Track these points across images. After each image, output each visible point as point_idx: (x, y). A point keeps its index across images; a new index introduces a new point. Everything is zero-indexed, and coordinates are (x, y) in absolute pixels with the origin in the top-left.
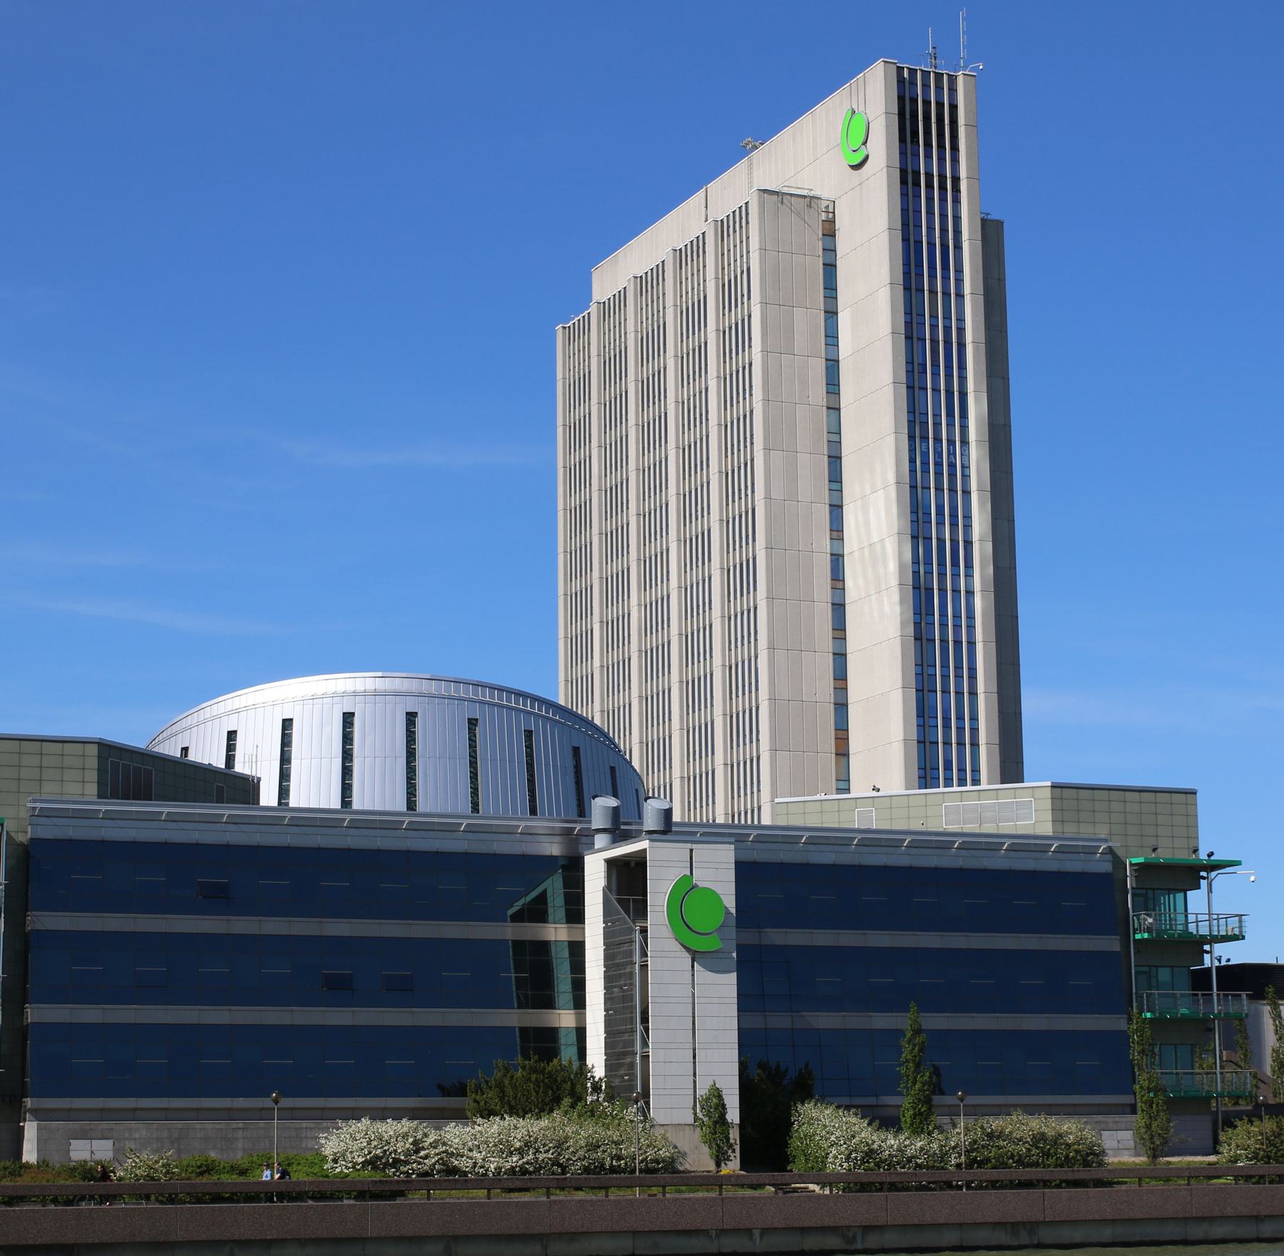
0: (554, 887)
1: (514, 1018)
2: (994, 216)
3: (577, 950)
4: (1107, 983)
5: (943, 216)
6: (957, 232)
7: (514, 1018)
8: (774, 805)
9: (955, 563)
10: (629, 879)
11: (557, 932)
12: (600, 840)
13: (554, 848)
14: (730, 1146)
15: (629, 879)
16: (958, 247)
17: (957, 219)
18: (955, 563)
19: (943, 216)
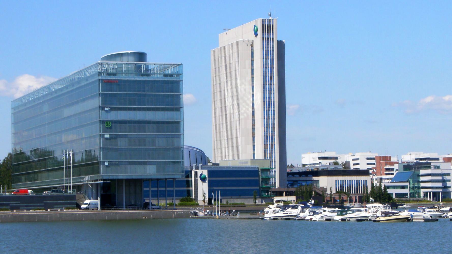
0: (190, 173)
1: (186, 189)
2: (279, 40)
3: (192, 181)
4: (256, 183)
5: (270, 45)
6: (273, 48)
7: (186, 189)
8: (148, 191)
9: (271, 105)
10: (196, 173)
11: (190, 179)
12: (194, 169)
13: (190, 170)
14: (320, 163)
15: (196, 173)
16: (273, 50)
17: (273, 45)
18: (271, 105)
19: (270, 45)
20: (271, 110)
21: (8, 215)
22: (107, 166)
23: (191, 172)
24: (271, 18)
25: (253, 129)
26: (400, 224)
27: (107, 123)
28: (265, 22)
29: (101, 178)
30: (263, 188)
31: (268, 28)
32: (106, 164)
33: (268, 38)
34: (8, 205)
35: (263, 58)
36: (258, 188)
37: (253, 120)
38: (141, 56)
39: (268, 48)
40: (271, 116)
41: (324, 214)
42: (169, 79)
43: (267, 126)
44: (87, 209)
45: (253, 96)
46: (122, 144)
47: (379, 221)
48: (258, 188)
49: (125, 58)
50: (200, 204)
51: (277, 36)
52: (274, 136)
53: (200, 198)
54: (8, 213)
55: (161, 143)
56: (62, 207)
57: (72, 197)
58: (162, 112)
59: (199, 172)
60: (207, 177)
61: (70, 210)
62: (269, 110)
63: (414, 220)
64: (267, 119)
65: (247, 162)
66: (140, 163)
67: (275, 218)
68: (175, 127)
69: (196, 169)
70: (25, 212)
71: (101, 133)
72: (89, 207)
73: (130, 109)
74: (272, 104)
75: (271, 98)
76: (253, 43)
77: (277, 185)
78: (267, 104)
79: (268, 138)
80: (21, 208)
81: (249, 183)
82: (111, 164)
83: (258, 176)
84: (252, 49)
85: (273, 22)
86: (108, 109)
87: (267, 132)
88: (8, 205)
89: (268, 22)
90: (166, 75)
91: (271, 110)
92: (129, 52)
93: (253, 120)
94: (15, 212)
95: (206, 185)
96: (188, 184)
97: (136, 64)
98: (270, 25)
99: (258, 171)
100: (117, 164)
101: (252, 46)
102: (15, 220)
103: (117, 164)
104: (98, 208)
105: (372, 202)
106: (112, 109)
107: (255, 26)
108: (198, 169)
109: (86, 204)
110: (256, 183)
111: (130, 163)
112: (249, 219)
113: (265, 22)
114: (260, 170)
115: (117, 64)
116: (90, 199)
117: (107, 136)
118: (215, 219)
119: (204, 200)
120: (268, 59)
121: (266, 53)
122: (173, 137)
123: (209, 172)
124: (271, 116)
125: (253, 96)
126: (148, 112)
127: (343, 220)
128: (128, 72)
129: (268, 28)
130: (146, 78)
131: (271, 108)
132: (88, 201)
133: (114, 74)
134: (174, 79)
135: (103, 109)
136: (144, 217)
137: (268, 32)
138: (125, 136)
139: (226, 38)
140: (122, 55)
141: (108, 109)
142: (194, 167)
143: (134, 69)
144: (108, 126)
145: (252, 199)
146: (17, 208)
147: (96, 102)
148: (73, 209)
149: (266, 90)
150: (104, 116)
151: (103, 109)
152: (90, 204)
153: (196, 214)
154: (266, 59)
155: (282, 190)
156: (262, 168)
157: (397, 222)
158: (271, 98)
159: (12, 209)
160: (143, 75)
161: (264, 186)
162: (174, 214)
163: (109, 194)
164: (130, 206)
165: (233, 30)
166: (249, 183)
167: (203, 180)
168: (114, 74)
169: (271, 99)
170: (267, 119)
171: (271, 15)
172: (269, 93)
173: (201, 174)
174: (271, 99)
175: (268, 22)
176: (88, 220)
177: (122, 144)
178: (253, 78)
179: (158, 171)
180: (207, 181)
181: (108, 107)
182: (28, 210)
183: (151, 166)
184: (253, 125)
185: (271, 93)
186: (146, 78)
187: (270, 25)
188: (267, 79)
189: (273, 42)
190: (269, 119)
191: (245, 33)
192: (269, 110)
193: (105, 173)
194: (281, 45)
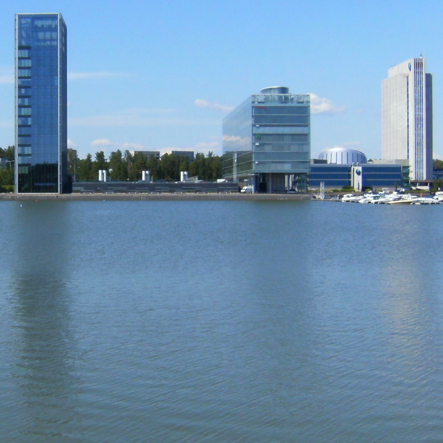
2: (428, 73)
4: (399, 176)
10: (354, 169)
12: (353, 166)
13: (350, 167)
15: (354, 169)
20: (421, 124)
21: (191, 196)
22: (257, 164)
23: (351, 168)
24: (421, 58)
25: (408, 137)
26: (406, 206)
27: (257, 135)
28: (417, 60)
29: (253, 172)
30: (404, 180)
31: (418, 65)
32: (257, 163)
33: (418, 72)
34: (194, 189)
35: (415, 86)
36: (400, 180)
37: (408, 131)
38: (284, 90)
39: (419, 79)
40: (421, 128)
41: (368, 198)
42: (262, 105)
43: (417, 135)
44: (245, 192)
45: (408, 113)
46: (268, 149)
47: (390, 204)
48: (400, 180)
49: (272, 91)
50: (356, 191)
51: (426, 70)
52: (423, 142)
53: (356, 187)
54: (193, 194)
55: (294, 149)
56: (229, 191)
57: (236, 185)
58: (270, 128)
59: (356, 168)
60: (361, 171)
61: (234, 193)
62: (419, 124)
63: (416, 204)
64: (417, 130)
65: (393, 162)
66: (280, 162)
67: (348, 201)
68: (305, 138)
69: (354, 166)
70: (204, 194)
71: (253, 142)
72: (246, 191)
73: (273, 126)
74: (422, 119)
75: (421, 115)
76: (408, 75)
77: (425, 178)
78: (418, 120)
79: (418, 144)
80: (156, 190)
81: (394, 176)
82: (260, 163)
83: (400, 171)
84: (408, 80)
85: (422, 60)
86: (258, 126)
87: (417, 139)
88: (194, 189)
89: (418, 60)
90: (299, 103)
91: (421, 124)
92: (275, 87)
93: (408, 131)
94: (198, 194)
95: (360, 177)
96: (349, 176)
97: (278, 95)
98: (418, 63)
99: (400, 168)
100: (264, 163)
101: (408, 78)
102: (226, 199)
103: (264, 163)
104: (252, 192)
105: (440, 191)
106: (260, 126)
107: (409, 64)
108: (356, 166)
109: (244, 189)
110: (399, 176)
111: (273, 162)
112: (336, 201)
113: (417, 60)
114: (401, 167)
115: (265, 95)
116: (247, 186)
117: (257, 144)
118: (321, 201)
119: (358, 188)
120: (419, 87)
121: (417, 83)
122: (303, 144)
123: (363, 168)
124: (421, 128)
125: (408, 113)
126: (292, 128)
127: (376, 203)
128: (274, 101)
129: (418, 65)
130: (284, 105)
131: (421, 122)
132: (245, 188)
133: (263, 103)
134: (304, 105)
135: (255, 125)
136: (281, 199)
137: (418, 68)
138: (269, 144)
139: (393, 72)
140: (271, 89)
141: (258, 126)
142: (353, 164)
143: (276, 98)
144: (257, 137)
145: (394, 188)
146: (200, 191)
147: (250, 122)
148: (235, 192)
149: (417, 109)
150: (256, 131)
151: (255, 125)
152: (246, 189)
153: (315, 197)
154: (417, 87)
155: (427, 181)
156: (403, 165)
157: (400, 205)
158: (421, 115)
159: (196, 192)
160: (282, 103)
161: (405, 179)
162: (302, 197)
163: (263, 183)
164: (275, 191)
165: (396, 67)
166: (394, 176)
167: (358, 173)
168: (263, 103)
169: (421, 116)
170: (417, 130)
171: (421, 55)
172: (419, 111)
173: (357, 170)
174: (421, 116)
175: (418, 60)
176: (246, 199)
177: (268, 149)
178: (408, 101)
179: (292, 167)
180: (361, 175)
181: (258, 125)
182: (206, 192)
183: (287, 164)
184: (408, 134)
185: (421, 111)
186: (284, 105)
187: (418, 63)
188: (418, 102)
189: (422, 74)
190: (419, 130)
191: (403, 69)
192: (419, 124)
193: (256, 168)
194: (429, 77)
